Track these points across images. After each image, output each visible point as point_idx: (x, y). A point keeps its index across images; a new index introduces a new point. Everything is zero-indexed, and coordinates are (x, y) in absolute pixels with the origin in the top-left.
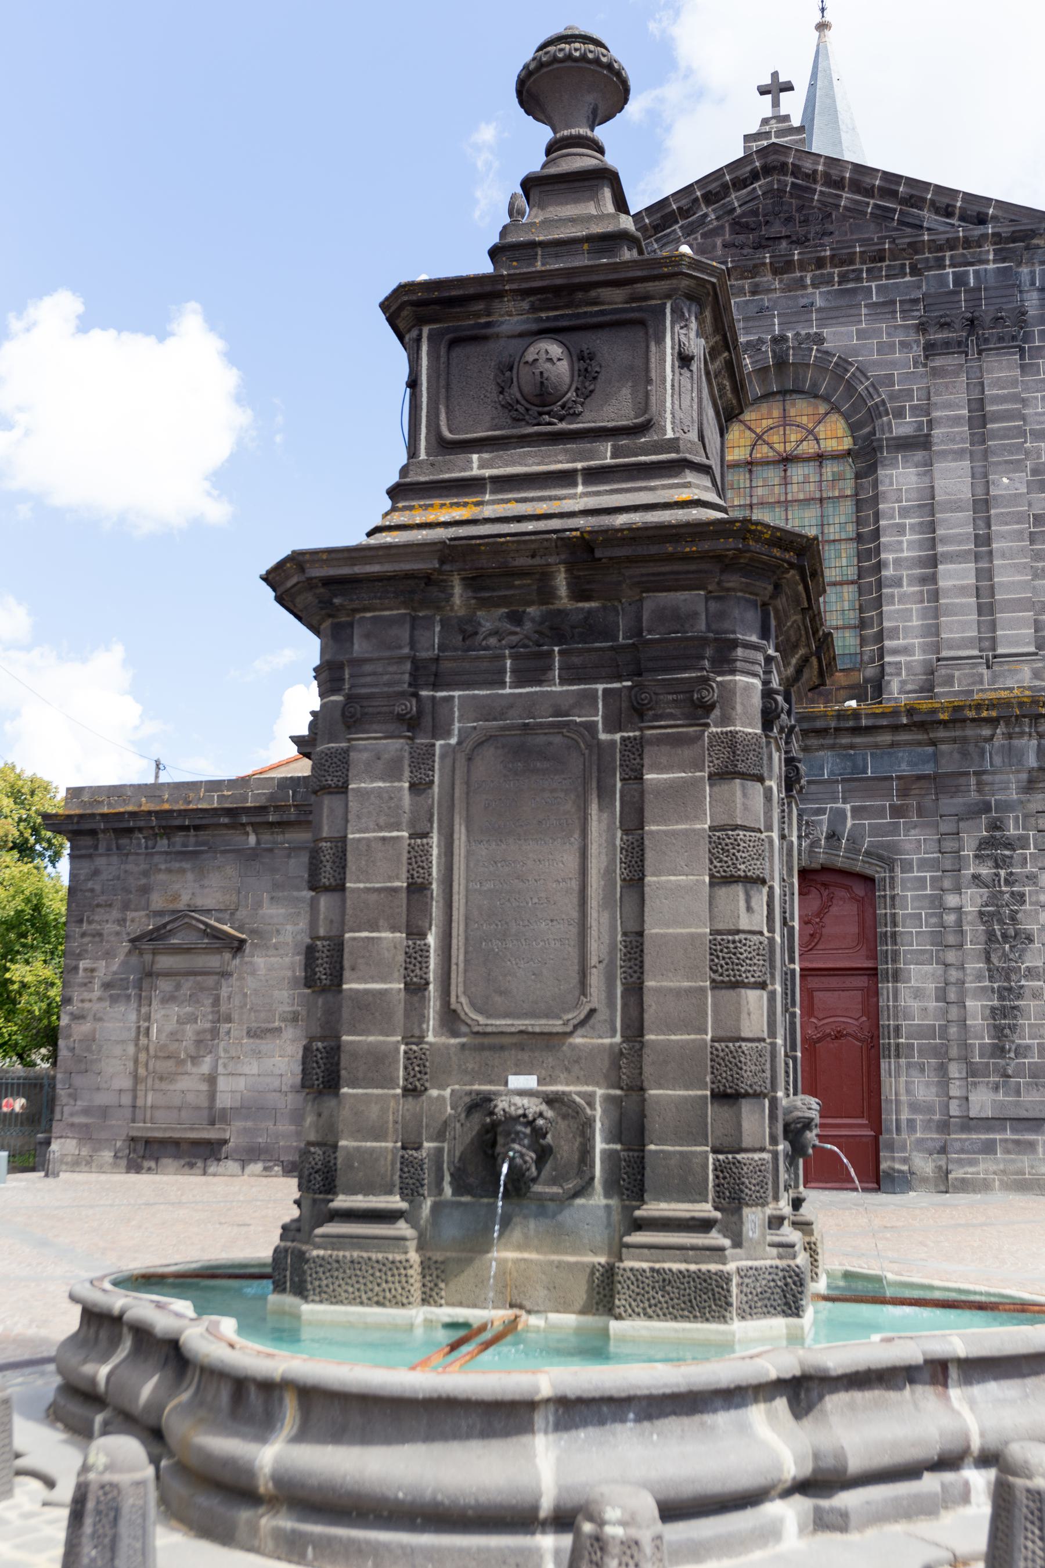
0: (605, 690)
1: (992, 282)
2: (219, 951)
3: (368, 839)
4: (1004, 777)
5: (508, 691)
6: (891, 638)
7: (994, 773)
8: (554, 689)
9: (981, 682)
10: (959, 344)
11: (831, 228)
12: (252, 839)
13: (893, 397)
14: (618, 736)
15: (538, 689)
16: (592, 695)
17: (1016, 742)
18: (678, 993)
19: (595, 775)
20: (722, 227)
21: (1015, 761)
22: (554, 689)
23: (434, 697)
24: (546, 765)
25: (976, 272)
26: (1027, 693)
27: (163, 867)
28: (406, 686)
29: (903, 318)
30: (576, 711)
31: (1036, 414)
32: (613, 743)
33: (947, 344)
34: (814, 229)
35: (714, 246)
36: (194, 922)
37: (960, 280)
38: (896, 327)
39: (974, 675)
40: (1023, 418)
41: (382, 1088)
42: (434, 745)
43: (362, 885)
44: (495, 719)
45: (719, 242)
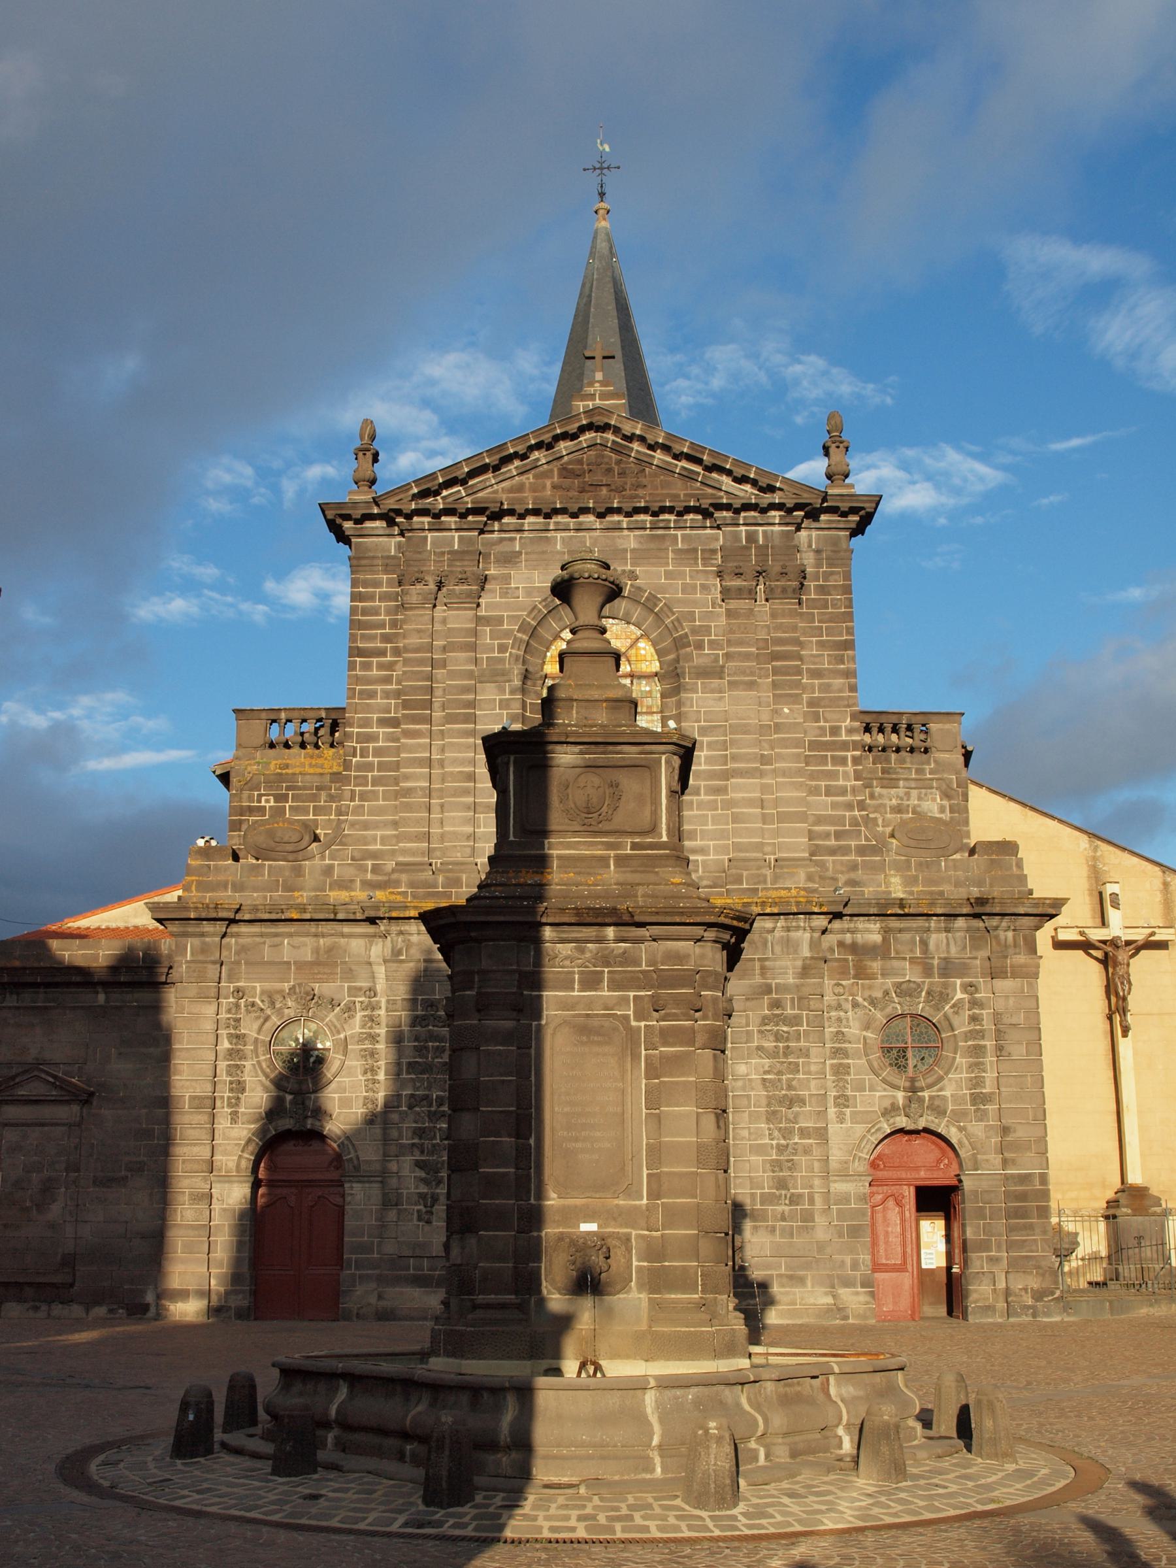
1: (777, 542)
2: (68, 1102)
4: (783, 963)
5: (576, 993)
6: (690, 839)
7: (775, 960)
9: (765, 882)
10: (750, 591)
11: (644, 481)
12: (101, 998)
13: (695, 631)
14: (643, 1024)
16: (627, 999)
17: (793, 934)
18: (681, 1175)
20: (552, 471)
21: (791, 950)
24: (600, 1039)
25: (764, 532)
27: (12, 1022)
29: (704, 565)
31: (812, 655)
33: (740, 590)
34: (630, 481)
35: (544, 487)
36: (43, 1076)
37: (751, 537)
38: (697, 571)
39: (759, 875)
40: (801, 658)
45: (548, 483)
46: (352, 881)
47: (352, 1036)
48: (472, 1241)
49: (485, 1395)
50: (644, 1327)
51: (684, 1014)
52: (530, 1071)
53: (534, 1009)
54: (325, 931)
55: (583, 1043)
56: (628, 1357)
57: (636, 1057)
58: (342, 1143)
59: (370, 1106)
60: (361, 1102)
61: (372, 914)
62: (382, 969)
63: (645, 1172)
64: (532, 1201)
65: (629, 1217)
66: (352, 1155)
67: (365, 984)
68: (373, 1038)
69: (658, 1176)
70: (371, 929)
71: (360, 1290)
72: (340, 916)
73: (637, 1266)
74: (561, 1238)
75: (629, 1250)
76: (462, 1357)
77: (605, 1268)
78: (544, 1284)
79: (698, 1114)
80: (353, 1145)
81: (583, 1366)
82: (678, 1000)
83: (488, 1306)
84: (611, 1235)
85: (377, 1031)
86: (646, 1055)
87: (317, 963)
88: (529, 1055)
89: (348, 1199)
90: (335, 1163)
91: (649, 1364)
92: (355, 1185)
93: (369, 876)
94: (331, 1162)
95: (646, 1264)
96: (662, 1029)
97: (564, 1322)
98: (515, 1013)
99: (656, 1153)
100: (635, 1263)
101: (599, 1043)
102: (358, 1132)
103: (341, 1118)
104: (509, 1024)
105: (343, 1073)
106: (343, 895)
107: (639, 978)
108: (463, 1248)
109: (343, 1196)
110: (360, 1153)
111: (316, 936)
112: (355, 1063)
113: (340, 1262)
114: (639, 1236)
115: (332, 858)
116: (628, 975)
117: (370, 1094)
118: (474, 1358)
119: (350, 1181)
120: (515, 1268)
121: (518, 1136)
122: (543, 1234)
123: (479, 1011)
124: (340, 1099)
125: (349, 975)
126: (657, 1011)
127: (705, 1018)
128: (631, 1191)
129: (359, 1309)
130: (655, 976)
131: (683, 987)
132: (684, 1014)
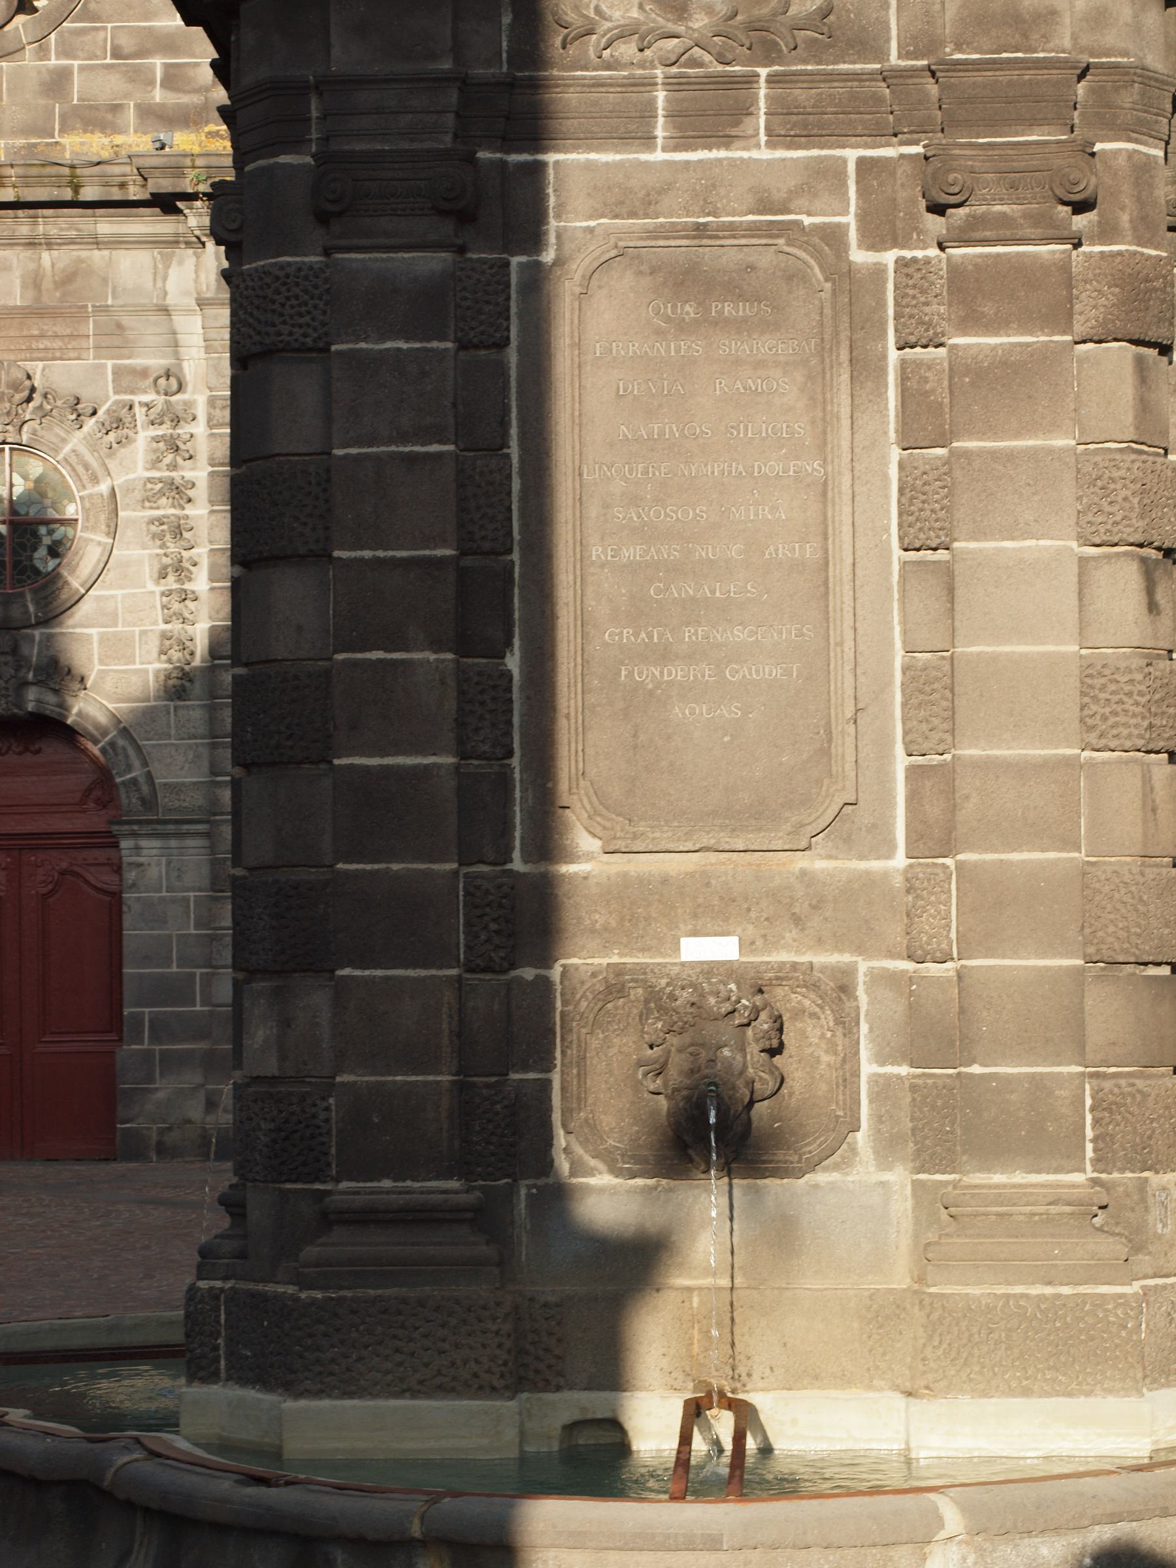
0: (861, 162)
3: (376, 457)
5: (659, 156)
8: (755, 154)
14: (889, 257)
15: (722, 154)
16: (836, 172)
18: (1022, 770)
19: (844, 335)
22: (755, 154)
23: (503, 164)
24: (744, 310)
26: (840, 750)
28: (448, 138)
30: (802, 202)
32: (878, 272)
41: (425, 966)
42: (507, 264)
43: (367, 554)
44: (633, 214)
46: (116, 108)
47: (129, 489)
48: (315, 1002)
49: (339, 1556)
50: (900, 1279)
51: (1036, 220)
52: (504, 424)
53: (511, 213)
54: (54, 231)
55: (683, 328)
56: (844, 1380)
57: (865, 369)
58: (112, 744)
59: (176, 655)
60: (154, 645)
61: (165, 185)
62: (197, 321)
63: (901, 762)
64: (517, 864)
65: (846, 912)
66: (137, 773)
67: (157, 363)
68: (179, 491)
69: (946, 776)
70: (164, 226)
71: (163, 1088)
72: (89, 193)
73: (875, 1079)
74: (615, 985)
75: (847, 1024)
76: (291, 1388)
77: (765, 1083)
78: (561, 1139)
79: (1083, 561)
80: (138, 749)
81: (695, 1411)
82: (1014, 173)
83: (367, 1217)
84: (785, 975)
85: (189, 475)
86: (903, 364)
87: (35, 312)
88: (501, 370)
89: (130, 876)
90: (97, 793)
91: (916, 1405)
92: (144, 843)
93: (158, 95)
94: (89, 790)
95: (904, 1070)
96: (956, 272)
97: (635, 1262)
98: (447, 228)
99: (937, 696)
100: (868, 1068)
101: (740, 326)
102: (148, 716)
103: (108, 685)
104: (434, 262)
105: (107, 577)
106: (96, 144)
107: (878, 99)
108: (286, 1023)
109: (118, 869)
110: (156, 768)
111: (32, 244)
112: (138, 554)
113: (114, 1023)
114: (879, 979)
115: (66, 51)
116: (840, 89)
117: (176, 627)
118: (319, 1394)
119: (134, 835)
120: (461, 1087)
121: (464, 647)
122: (556, 973)
123: (323, 219)
124: (103, 639)
125: (116, 338)
126: (938, 209)
127: (1107, 232)
128: (847, 826)
129: (161, 1132)
130: (933, 89)
131: (1033, 123)
132: (1036, 220)
